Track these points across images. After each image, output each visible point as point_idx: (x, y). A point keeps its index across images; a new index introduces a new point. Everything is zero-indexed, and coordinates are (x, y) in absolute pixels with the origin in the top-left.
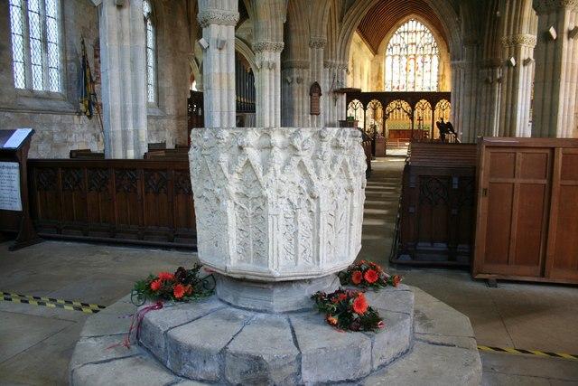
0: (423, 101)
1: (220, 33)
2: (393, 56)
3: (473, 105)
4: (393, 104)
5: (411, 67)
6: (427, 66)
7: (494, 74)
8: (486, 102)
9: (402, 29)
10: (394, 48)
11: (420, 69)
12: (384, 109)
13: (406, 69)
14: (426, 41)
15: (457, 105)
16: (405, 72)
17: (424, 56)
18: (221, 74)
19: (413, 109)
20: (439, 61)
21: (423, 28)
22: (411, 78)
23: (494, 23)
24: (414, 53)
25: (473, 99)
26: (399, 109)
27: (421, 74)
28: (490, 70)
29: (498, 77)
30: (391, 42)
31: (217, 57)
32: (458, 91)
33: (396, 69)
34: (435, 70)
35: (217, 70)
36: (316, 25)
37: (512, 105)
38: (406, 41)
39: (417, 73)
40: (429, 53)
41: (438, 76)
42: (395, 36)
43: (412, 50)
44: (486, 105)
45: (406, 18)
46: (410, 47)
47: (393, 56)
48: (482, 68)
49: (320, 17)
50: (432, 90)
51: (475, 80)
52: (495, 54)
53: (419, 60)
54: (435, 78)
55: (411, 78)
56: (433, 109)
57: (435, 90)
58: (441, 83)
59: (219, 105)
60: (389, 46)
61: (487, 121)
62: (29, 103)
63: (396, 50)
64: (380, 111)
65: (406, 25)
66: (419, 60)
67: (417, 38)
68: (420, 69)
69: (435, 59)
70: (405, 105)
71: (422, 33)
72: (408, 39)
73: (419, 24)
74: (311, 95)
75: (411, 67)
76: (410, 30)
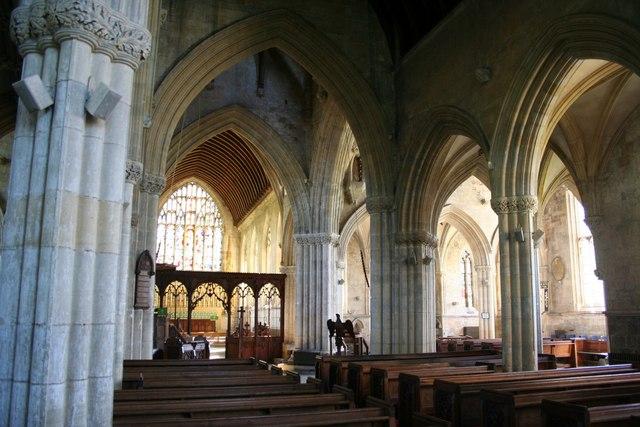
0: (177, 283)
1: (96, 71)
2: (166, 225)
3: (386, 296)
4: (203, 289)
5: (189, 240)
6: (209, 241)
7: (417, 252)
8: (409, 290)
9: (179, 193)
10: (169, 215)
11: (200, 243)
12: (189, 296)
13: (183, 243)
14: (208, 211)
15: (305, 291)
16: (181, 246)
17: (205, 227)
18: (83, 199)
19: (230, 296)
20: (223, 235)
21: (204, 194)
22: (189, 253)
23: (419, 184)
24: (193, 223)
25: (387, 286)
26: (210, 295)
27: (201, 249)
28: (412, 246)
29: (423, 257)
30: (165, 206)
31: (79, 145)
32: (305, 273)
33: (170, 241)
34: (218, 245)
35: (75, 186)
36: (153, 155)
37: (523, 299)
38: (183, 207)
39: (196, 248)
40: (212, 224)
41: (222, 252)
42: (170, 201)
43: (190, 220)
44: (409, 294)
45: (185, 181)
46: (188, 216)
47: (166, 225)
48: (399, 243)
49: (159, 145)
50: (215, 270)
51: (386, 260)
52: (417, 224)
53: (199, 232)
54: (218, 255)
55: (189, 253)
56: (256, 296)
57: (217, 269)
58: (225, 261)
59: (69, 301)
60: (162, 213)
61: (412, 320)
62: (287, 245)
63: (171, 218)
64: (183, 297)
65: (184, 188)
66: (199, 232)
67: (198, 206)
68: (200, 243)
69: (218, 232)
70: (219, 290)
71: (204, 201)
72: (187, 205)
73: (200, 189)
74: (137, 273)
75: (189, 240)
76: (189, 195)
